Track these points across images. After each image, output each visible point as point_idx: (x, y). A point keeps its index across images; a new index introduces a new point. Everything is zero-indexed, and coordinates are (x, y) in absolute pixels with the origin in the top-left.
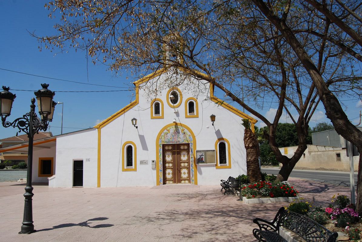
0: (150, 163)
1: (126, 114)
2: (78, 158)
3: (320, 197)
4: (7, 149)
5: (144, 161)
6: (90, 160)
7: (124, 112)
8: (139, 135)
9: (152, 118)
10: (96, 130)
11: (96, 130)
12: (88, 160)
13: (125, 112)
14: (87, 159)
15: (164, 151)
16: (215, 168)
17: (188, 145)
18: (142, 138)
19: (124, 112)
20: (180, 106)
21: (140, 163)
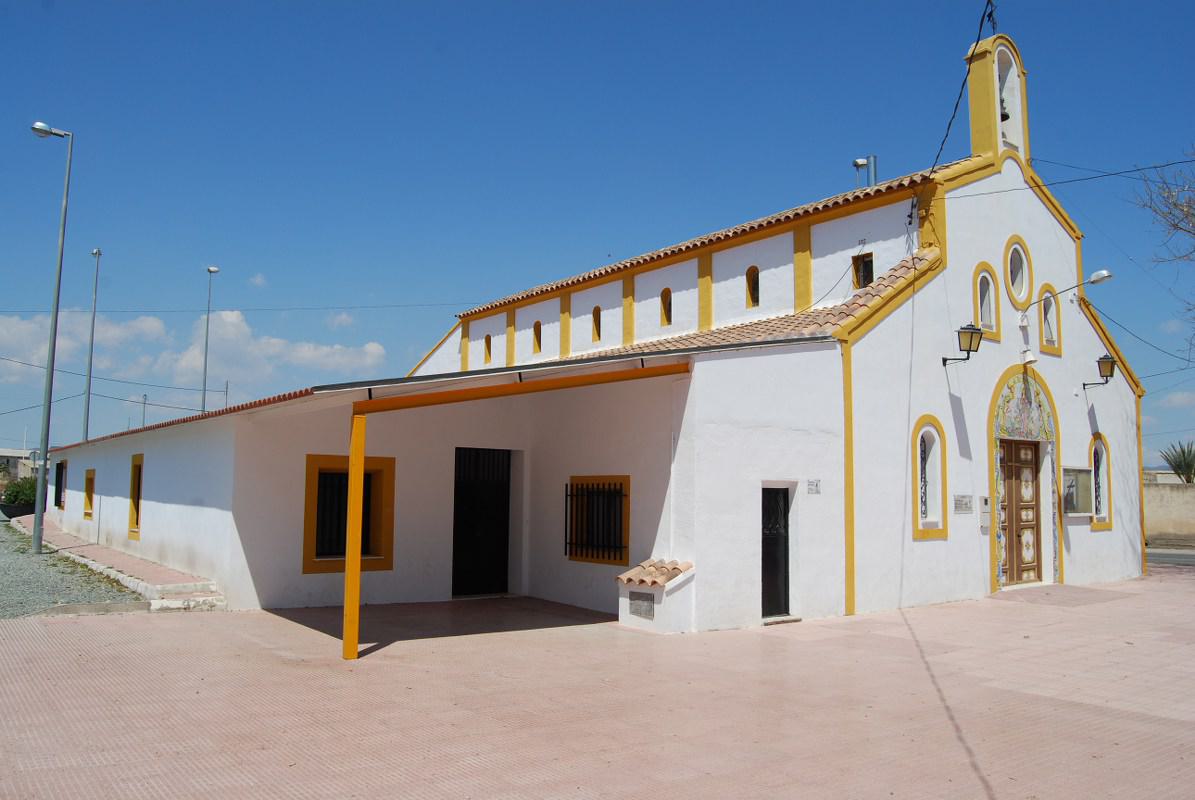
0: (977, 505)
1: (919, 296)
2: (777, 478)
3: (219, 603)
4: (588, 372)
5: (963, 497)
6: (822, 487)
7: (914, 292)
8: (950, 394)
9: (311, 459)
10: (835, 348)
11: (835, 348)
12: (814, 487)
13: (918, 291)
14: (810, 483)
15: (41, 553)
16: (1088, 527)
17: (1035, 447)
18: (956, 403)
19: (911, 288)
20: (1011, 307)
21: (956, 507)
